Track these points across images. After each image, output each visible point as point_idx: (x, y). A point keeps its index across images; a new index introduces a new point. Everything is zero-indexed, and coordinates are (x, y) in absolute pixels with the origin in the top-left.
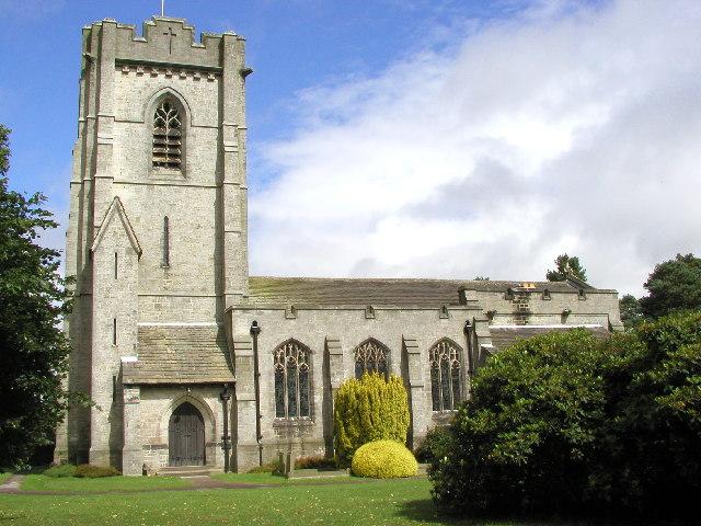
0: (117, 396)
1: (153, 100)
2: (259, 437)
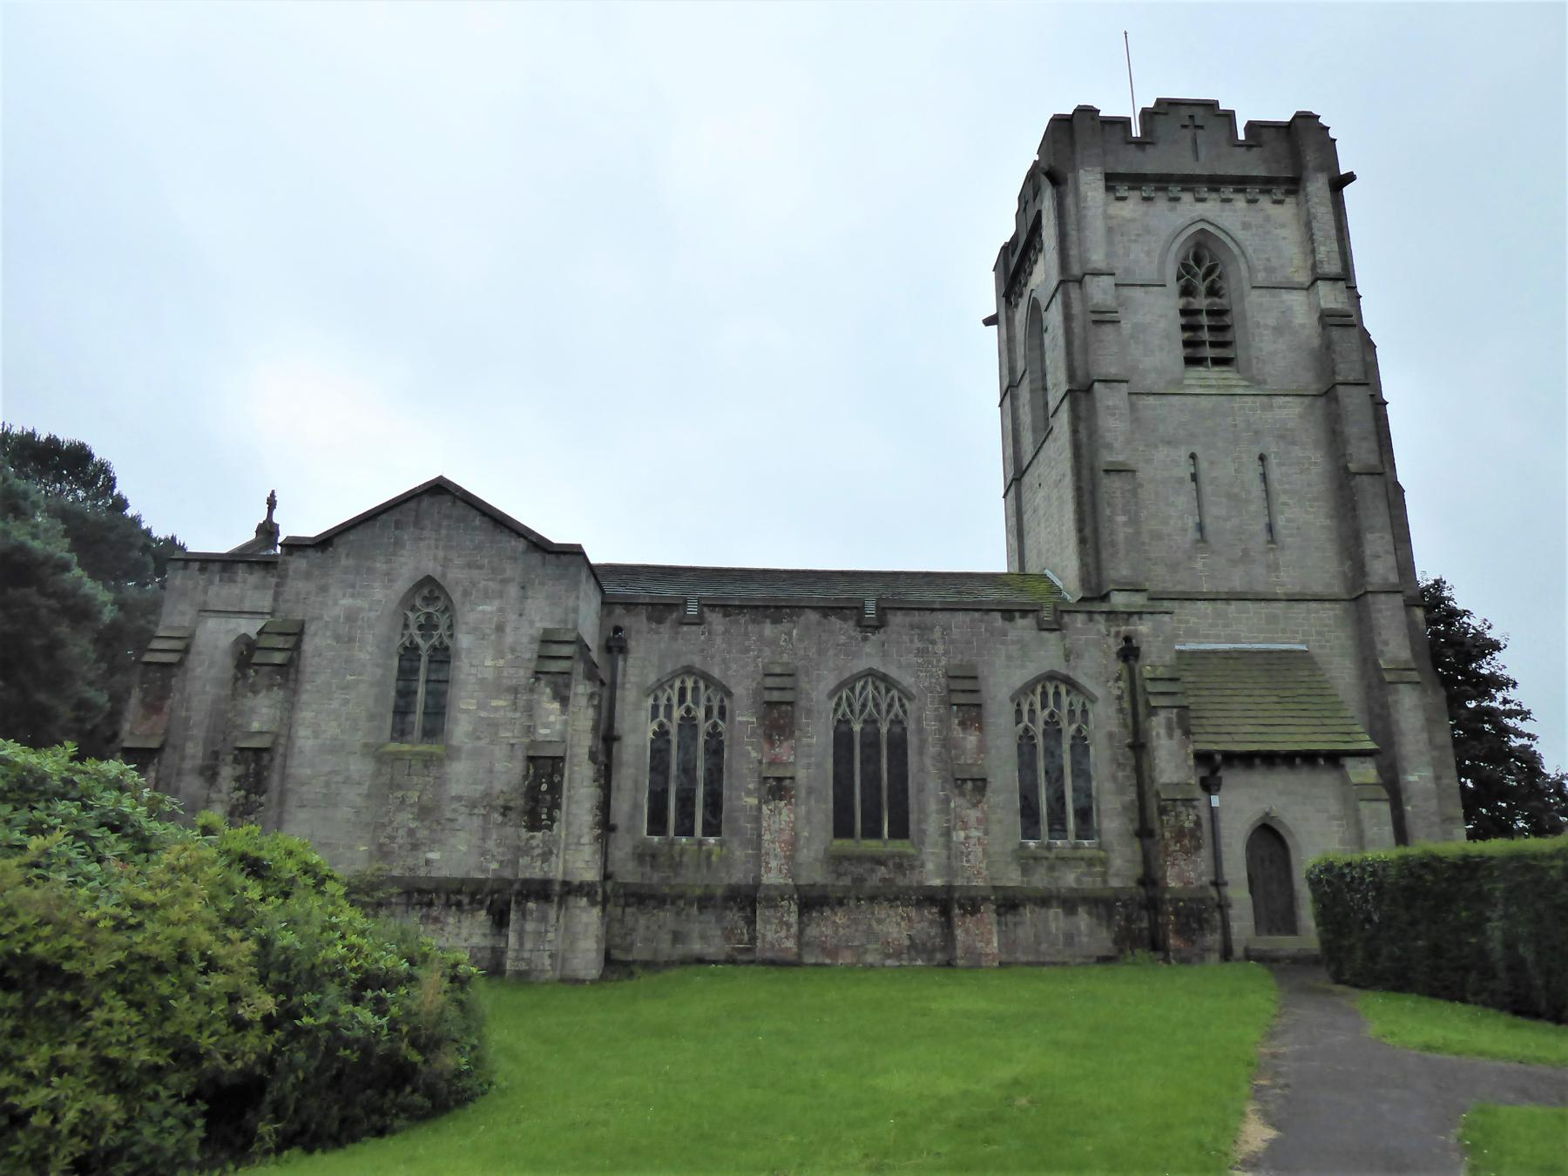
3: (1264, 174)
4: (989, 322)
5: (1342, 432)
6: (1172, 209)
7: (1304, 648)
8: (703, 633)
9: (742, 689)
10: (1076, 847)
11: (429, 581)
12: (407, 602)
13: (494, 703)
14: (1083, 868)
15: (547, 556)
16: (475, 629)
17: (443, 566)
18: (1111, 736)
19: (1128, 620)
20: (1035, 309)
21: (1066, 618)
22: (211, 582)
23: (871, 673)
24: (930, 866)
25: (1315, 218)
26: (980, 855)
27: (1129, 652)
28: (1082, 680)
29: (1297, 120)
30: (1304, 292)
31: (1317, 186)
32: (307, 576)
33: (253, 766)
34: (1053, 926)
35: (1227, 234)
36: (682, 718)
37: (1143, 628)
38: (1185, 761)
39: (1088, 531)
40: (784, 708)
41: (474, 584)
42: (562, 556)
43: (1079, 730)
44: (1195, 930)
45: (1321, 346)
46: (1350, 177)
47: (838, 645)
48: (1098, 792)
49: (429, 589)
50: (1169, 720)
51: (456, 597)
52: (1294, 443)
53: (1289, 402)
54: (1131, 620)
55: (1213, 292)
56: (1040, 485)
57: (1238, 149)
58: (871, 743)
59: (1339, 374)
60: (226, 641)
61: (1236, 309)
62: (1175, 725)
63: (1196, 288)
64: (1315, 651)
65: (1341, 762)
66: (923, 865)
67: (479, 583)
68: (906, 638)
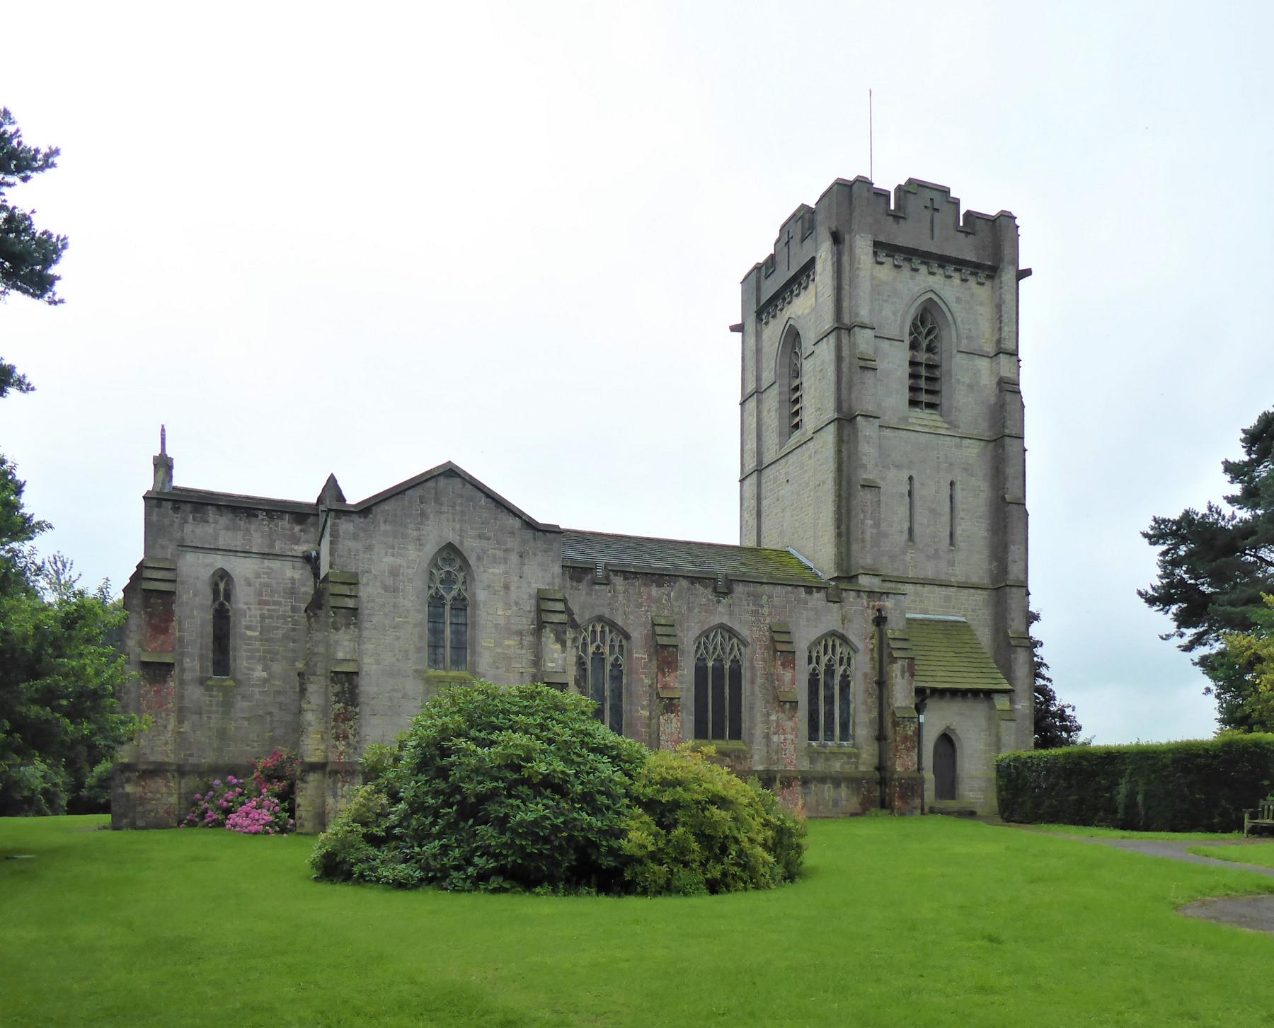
3: (974, 259)
4: (734, 329)
5: (1004, 472)
6: (913, 278)
7: (964, 620)
8: (610, 592)
9: (638, 634)
10: (840, 746)
11: (450, 547)
12: (434, 563)
13: (507, 642)
14: (845, 759)
15: (537, 533)
16: (489, 586)
17: (460, 536)
18: (866, 675)
19: (880, 598)
20: (792, 337)
21: (844, 594)
22: (186, 522)
23: (722, 627)
24: (756, 757)
25: (1004, 303)
26: (793, 750)
27: (880, 621)
28: (852, 637)
29: (1001, 218)
30: (989, 359)
32: (355, 537)
33: (347, 685)
34: (826, 795)
36: (594, 653)
37: (889, 603)
38: (910, 693)
39: (843, 528)
40: (671, 649)
41: (484, 552)
42: (547, 534)
43: (845, 671)
44: (909, 796)
45: (995, 404)
46: (1028, 272)
47: (701, 605)
48: (855, 711)
49: (451, 552)
50: (903, 666)
51: (472, 560)
52: (972, 475)
53: (971, 444)
54: (882, 598)
55: (930, 349)
56: (788, 481)
57: (959, 233)
58: (718, 671)
59: (1007, 428)
60: (206, 574)
61: (945, 366)
62: (906, 670)
63: (920, 344)
64: (970, 622)
65: (992, 696)
66: (752, 757)
67: (488, 550)
68: (744, 602)
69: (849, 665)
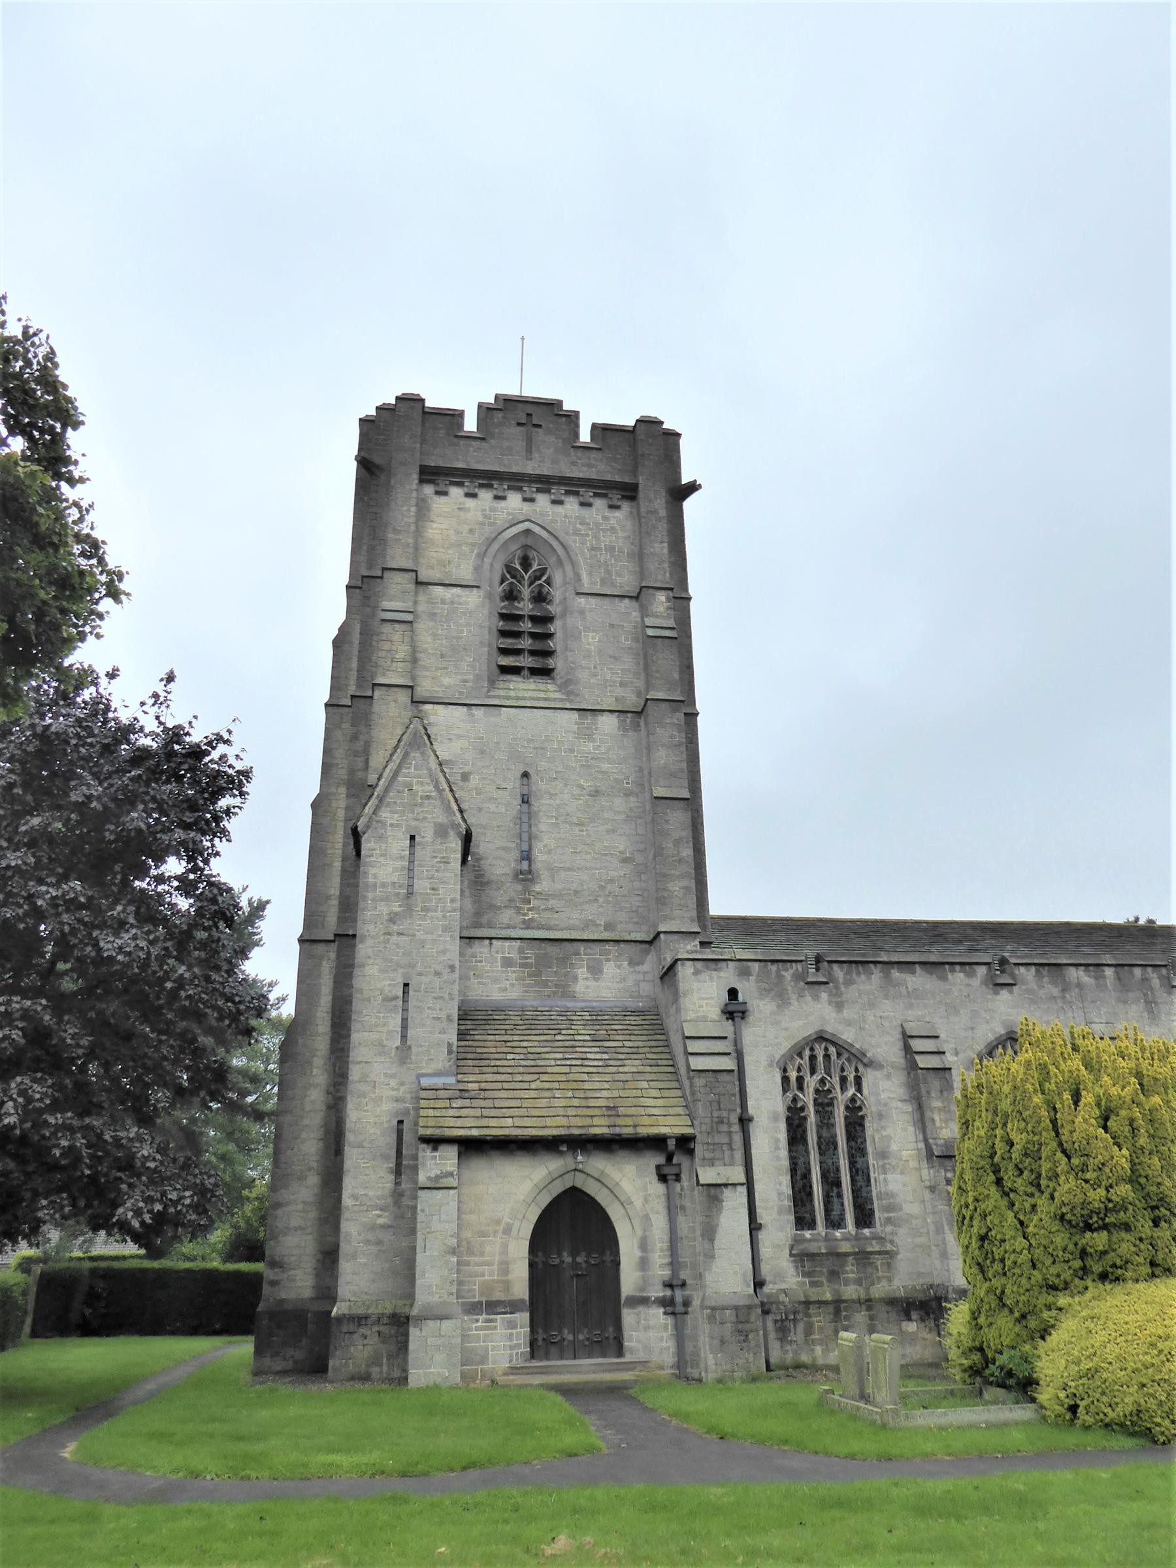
0: (401, 1166)
1: (496, 546)
2: (759, 1284)
31: (654, 499)
35: (556, 538)
46: (693, 487)
55: (540, 598)
69: (859, 1088)
